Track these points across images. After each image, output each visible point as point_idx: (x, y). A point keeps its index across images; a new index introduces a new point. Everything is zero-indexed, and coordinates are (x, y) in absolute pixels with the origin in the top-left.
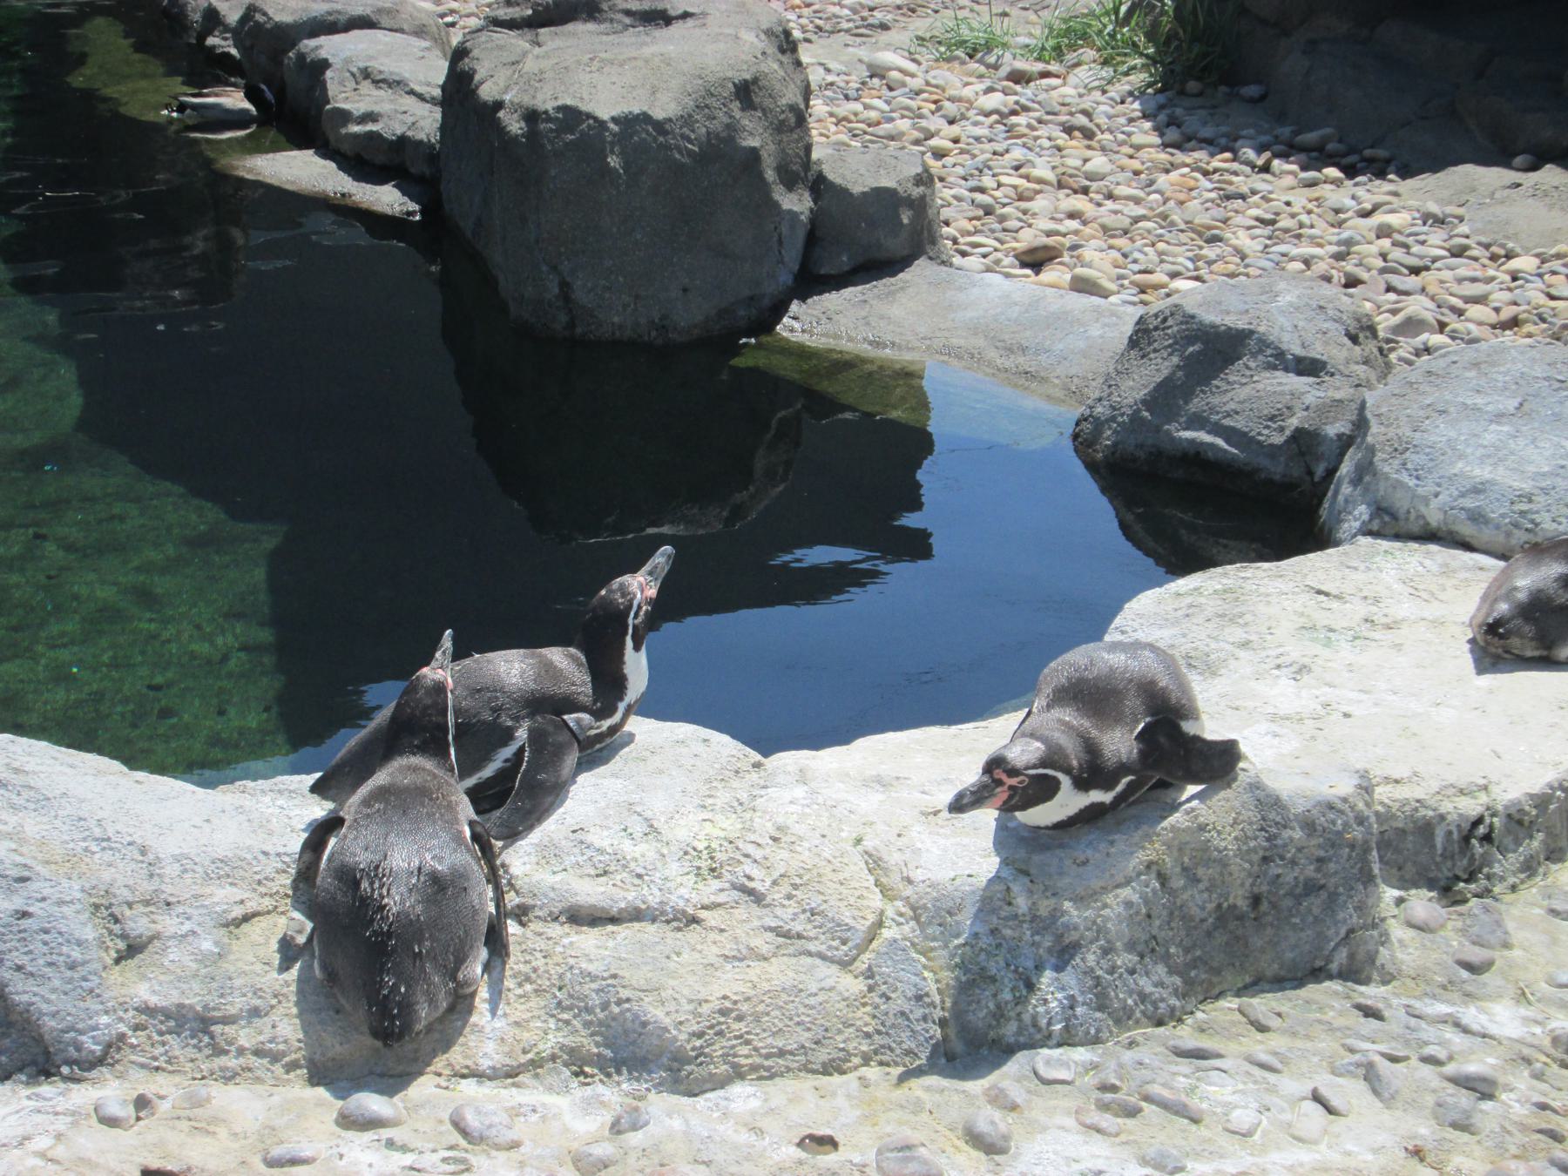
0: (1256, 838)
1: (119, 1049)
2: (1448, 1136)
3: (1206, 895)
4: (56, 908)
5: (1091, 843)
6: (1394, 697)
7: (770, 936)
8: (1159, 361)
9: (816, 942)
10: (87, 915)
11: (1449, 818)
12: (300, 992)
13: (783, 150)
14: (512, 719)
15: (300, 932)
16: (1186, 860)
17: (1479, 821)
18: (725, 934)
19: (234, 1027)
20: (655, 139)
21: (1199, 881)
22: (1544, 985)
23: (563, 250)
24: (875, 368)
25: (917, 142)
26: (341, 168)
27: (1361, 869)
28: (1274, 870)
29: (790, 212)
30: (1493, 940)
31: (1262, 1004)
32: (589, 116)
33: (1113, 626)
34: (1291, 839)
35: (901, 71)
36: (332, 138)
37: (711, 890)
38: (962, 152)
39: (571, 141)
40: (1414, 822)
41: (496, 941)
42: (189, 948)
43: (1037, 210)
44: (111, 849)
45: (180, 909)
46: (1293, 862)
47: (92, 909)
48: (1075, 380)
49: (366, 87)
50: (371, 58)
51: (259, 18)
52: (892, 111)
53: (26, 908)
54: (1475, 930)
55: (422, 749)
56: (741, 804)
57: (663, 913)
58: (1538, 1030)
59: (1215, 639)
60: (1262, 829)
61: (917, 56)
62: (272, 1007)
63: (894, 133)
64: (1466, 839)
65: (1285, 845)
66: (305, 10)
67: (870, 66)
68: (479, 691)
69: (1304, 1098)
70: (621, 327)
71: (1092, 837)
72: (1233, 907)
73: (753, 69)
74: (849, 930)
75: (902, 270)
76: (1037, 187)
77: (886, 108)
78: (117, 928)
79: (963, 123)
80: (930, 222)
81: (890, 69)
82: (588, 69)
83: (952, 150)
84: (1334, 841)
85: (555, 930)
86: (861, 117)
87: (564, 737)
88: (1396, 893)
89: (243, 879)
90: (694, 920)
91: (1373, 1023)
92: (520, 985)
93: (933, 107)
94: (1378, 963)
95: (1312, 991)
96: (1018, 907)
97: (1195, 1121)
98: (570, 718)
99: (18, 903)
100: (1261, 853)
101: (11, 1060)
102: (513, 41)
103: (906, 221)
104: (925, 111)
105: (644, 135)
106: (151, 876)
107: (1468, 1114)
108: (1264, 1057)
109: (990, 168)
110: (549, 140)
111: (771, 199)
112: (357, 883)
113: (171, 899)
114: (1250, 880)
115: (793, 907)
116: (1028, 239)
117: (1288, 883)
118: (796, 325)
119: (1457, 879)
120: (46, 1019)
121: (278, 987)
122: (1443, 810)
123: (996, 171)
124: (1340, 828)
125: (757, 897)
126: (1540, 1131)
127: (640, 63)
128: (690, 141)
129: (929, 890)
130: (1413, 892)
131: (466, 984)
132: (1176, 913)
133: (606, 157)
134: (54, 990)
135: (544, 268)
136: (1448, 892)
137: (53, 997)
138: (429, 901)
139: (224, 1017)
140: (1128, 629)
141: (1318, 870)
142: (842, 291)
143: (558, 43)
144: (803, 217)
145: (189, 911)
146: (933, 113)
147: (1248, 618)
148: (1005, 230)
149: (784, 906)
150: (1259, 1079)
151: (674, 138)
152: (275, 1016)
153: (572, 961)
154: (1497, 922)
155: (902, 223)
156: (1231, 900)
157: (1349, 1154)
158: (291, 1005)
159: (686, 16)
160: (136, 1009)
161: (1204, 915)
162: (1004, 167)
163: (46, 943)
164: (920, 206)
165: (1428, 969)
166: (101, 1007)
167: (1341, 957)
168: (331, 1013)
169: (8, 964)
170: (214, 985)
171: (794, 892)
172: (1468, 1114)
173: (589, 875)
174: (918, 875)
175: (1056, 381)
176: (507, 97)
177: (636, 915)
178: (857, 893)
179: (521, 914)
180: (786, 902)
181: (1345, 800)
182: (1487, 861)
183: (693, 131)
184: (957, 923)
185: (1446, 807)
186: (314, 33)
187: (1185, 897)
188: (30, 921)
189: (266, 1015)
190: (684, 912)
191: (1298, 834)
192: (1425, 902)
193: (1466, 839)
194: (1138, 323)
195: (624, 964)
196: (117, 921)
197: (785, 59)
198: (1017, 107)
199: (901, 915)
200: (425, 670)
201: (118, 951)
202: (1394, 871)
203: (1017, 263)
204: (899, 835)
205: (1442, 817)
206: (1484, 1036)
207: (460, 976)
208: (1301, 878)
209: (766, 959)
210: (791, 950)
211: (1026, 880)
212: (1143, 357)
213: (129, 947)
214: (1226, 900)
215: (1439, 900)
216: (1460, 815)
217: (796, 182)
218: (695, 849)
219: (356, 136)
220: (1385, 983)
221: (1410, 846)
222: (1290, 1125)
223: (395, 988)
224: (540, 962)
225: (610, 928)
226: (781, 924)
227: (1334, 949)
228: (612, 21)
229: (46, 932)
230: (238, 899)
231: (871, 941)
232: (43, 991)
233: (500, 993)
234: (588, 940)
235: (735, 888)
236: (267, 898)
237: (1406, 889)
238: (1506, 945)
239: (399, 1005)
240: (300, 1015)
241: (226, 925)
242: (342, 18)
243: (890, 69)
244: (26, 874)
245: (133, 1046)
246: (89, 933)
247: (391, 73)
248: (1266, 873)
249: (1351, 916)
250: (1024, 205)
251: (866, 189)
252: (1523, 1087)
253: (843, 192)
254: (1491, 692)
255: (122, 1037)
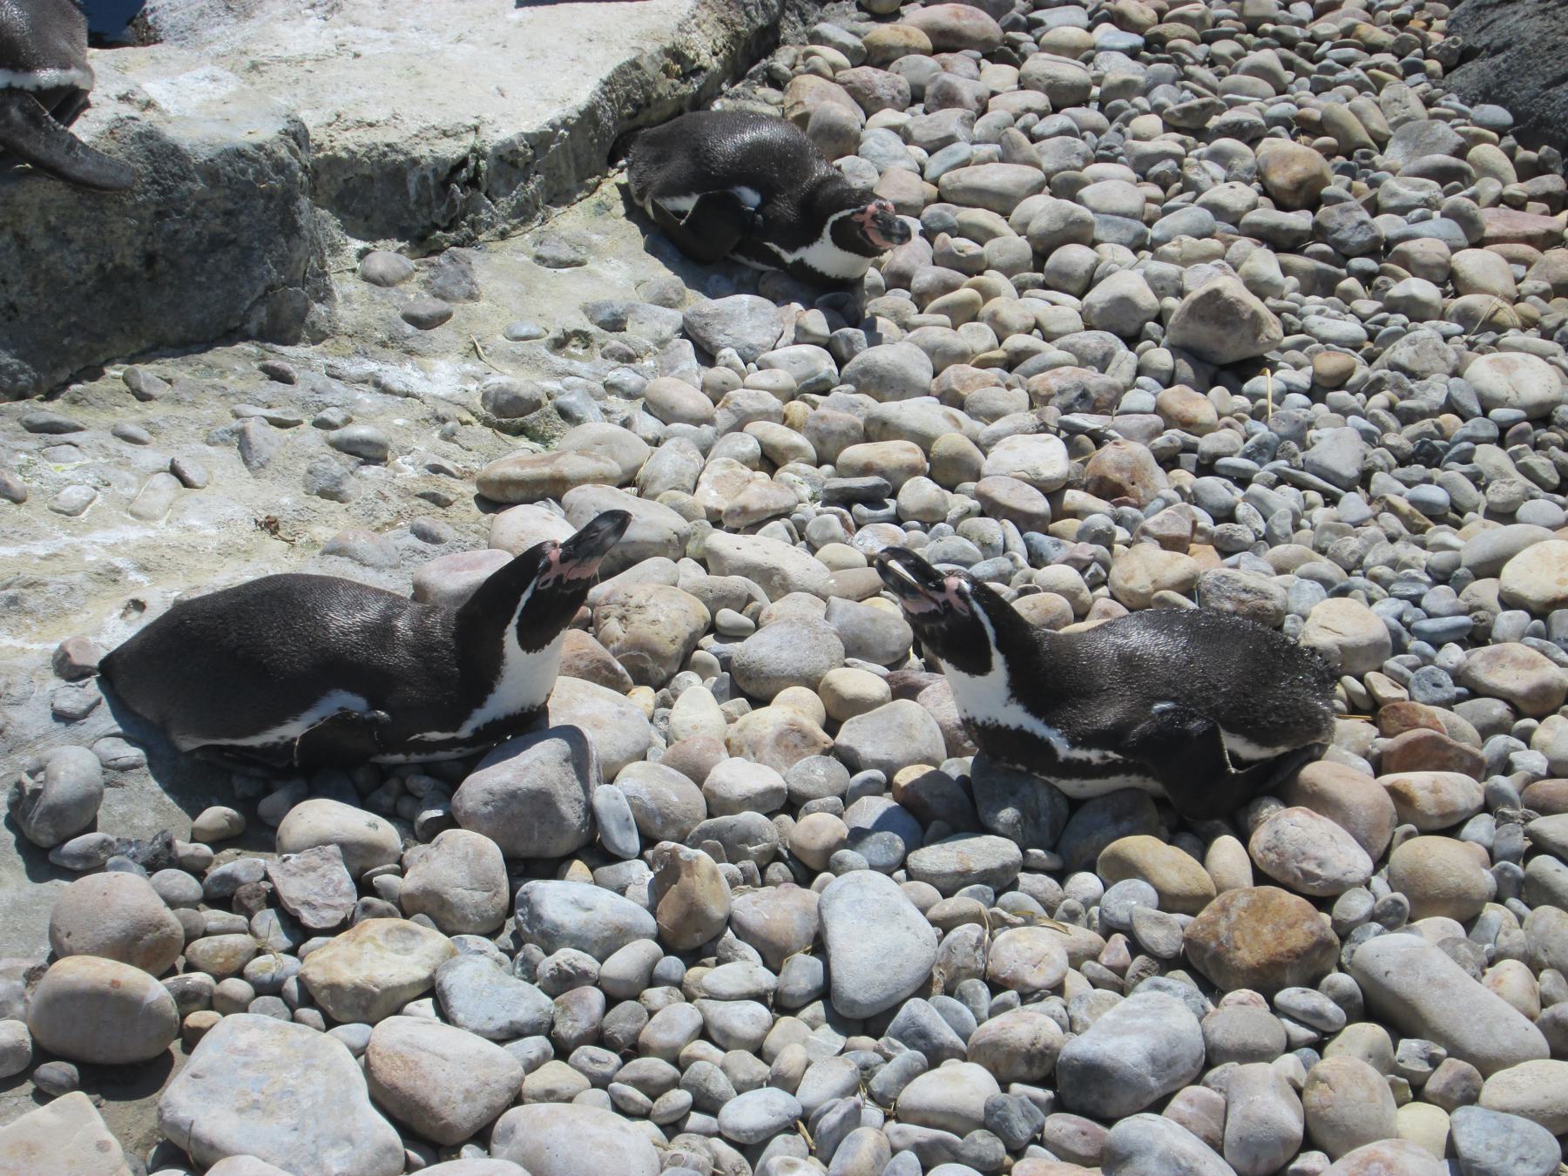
0: (145, 193)
2: (313, 505)
3: (82, 256)
6: (416, 35)
11: (423, 161)
16: (52, 219)
17: (463, 162)
22: (500, 338)
27: (282, 223)
28: (170, 225)
30: (456, 291)
31: (147, 373)
34: (191, 192)
40: (382, 168)
46: (194, 217)
54: (439, 281)
58: (472, 387)
60: (154, 182)
64: (444, 185)
65: (183, 199)
69: (160, 471)
72: (120, 268)
84: (243, 192)
88: (360, 245)
91: (278, 387)
94: (308, 321)
95: (219, 355)
97: (18, 501)
100: (153, 208)
107: (338, 481)
108: (131, 429)
114: (141, 238)
119: (437, 227)
122: (416, 154)
126: (423, 496)
130: (381, 242)
132: (41, 276)
136: (423, 243)
141: (226, 224)
150: (113, 452)
154: (463, 272)
156: (118, 261)
157: (189, 529)
161: (80, 277)
165: (369, 326)
167: (261, 315)
172: (338, 481)
181: (260, 147)
182: (472, 206)
185: (422, 151)
191: (199, 186)
192: (392, 254)
193: (444, 185)
202: (361, 221)
205: (415, 162)
206: (407, 395)
214: (110, 260)
215: (411, 250)
216: (436, 159)
220: (315, 342)
221: (378, 194)
222: (131, 501)
227: (251, 308)
237: (373, 240)
238: (472, 297)
249: (269, 272)
252: (422, 449)
254: (520, 24)
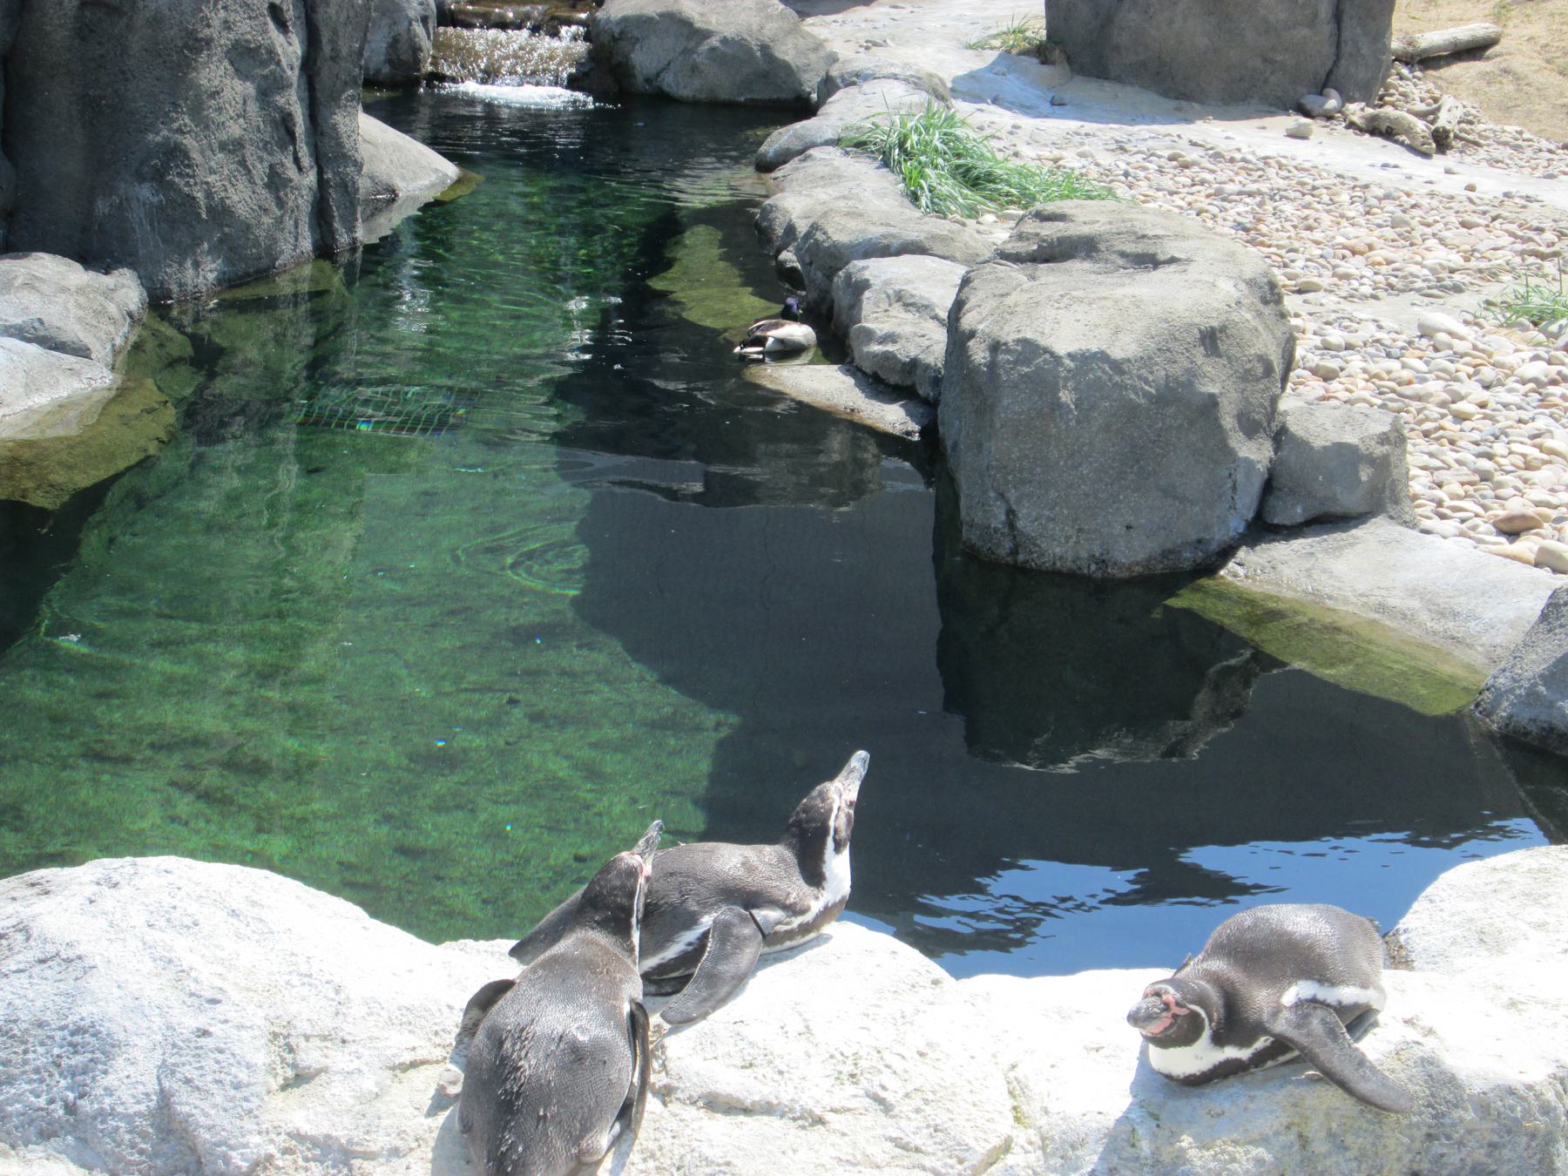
0: (1421, 1114)
1: (266, 1168)
4: (235, 1032)
5: (1231, 1096)
7: (889, 1145)
8: (1563, 636)
9: (933, 1158)
10: (264, 1041)
12: (440, 1139)
13: (1246, 399)
14: (698, 903)
15: (454, 1083)
16: (1334, 1125)
18: (846, 1138)
19: (373, 1163)
20: (1110, 379)
21: (1346, 1149)
23: (1010, 478)
24: (1305, 620)
25: (1443, 405)
26: (858, 385)
27: (1540, 1161)
29: (1246, 460)
32: (1046, 351)
33: (1424, 894)
34: (1461, 1120)
35: (1451, 334)
36: (856, 355)
37: (845, 1095)
38: (1485, 417)
39: (1026, 374)
41: (627, 1113)
42: (352, 1085)
43: (1536, 480)
44: (310, 985)
45: (353, 1048)
46: (1461, 1143)
47: (271, 1037)
48: (1499, 649)
49: (897, 310)
50: (909, 282)
51: (819, 236)
52: (1430, 372)
53: (207, 1027)
55: (602, 925)
56: (903, 1017)
57: (791, 1110)
59: (1514, 917)
60: (1429, 1105)
61: (1481, 320)
62: (411, 1150)
63: (1422, 393)
65: (1453, 1125)
66: (862, 231)
67: (1421, 326)
68: (672, 874)
70: (1061, 558)
71: (1233, 1090)
73: (1223, 317)
74: (968, 1150)
75: (1356, 527)
76: (1546, 457)
77: (1424, 368)
78: (289, 1058)
79: (1498, 389)
80: (1393, 481)
81: (1440, 330)
82: (1056, 305)
83: (1473, 415)
84: (1510, 1128)
85: (691, 1113)
86: (1393, 375)
87: (748, 930)
89: (422, 1028)
90: (820, 1121)
92: (645, 1160)
93: (1471, 370)
96: (1141, 1149)
98: (760, 914)
99: (202, 1021)
100: (1425, 1130)
101: (166, 1164)
102: (1013, 274)
103: (1364, 478)
104: (1462, 375)
105: (1099, 373)
106: (337, 1014)
109: (1507, 435)
110: (1006, 371)
111: (1226, 446)
112: (501, 1043)
113: (347, 1038)
114: (1410, 1156)
115: (918, 1120)
116: (1515, 506)
117: (1452, 1164)
118: (1241, 571)
120: (202, 1131)
121: (421, 1132)
123: (1511, 438)
124: (1519, 1115)
125: (885, 1106)
127: (1109, 303)
128: (1147, 382)
129: (1060, 1122)
131: (588, 1152)
133: (1059, 390)
134: (215, 1106)
135: (992, 494)
137: (213, 1112)
138: (564, 1068)
139: (365, 1153)
140: (1437, 899)
141: (1489, 1155)
142: (1292, 542)
143: (1051, 279)
144: (1259, 466)
145: (360, 1050)
146: (1470, 377)
147: (1553, 899)
148: (1497, 497)
149: (909, 1119)
151: (1131, 378)
152: (410, 1159)
153: (695, 1144)
155: (1360, 481)
158: (429, 1149)
159: (1173, 260)
160: (288, 1134)
162: (1522, 436)
163: (218, 1062)
164: (1382, 465)
166: (256, 1127)
168: (463, 1163)
169: (178, 1076)
170: (364, 1122)
171: (923, 1107)
173: (735, 1066)
174: (1053, 1108)
175: (1480, 649)
176: (981, 327)
177: (767, 1109)
178: (988, 1116)
179: (665, 1094)
180: (913, 1116)
181: (1530, 1088)
183: (1152, 373)
184: (1077, 1157)
186: (867, 255)
187: (1328, 1163)
188: (209, 1039)
189: (404, 1156)
190: (811, 1113)
191: (1470, 1115)
194: (1551, 597)
195: (741, 1153)
196: (291, 1050)
197: (1267, 311)
198: (1558, 378)
199: (1031, 1143)
200: (624, 854)
201: (285, 1079)
203: (1494, 530)
204: (1053, 1066)
207: (584, 1144)
208: (1469, 1161)
209: (878, 1167)
210: (906, 1162)
211: (1153, 1124)
212: (1550, 631)
213: (297, 1075)
217: (1257, 431)
218: (842, 1054)
219: (875, 355)
223: (513, 1147)
224: (666, 1142)
225: (742, 1118)
226: (901, 1135)
228: (1107, 261)
229: (221, 1051)
230: (410, 1045)
231: (991, 1165)
232: (205, 1105)
233: (624, 1165)
234: (719, 1126)
235: (868, 1096)
236: (439, 1049)
239: (515, 1164)
240: (433, 1161)
241: (393, 1068)
242: (896, 243)
243: (1440, 330)
244: (219, 997)
245: (278, 1168)
246: (261, 1058)
247: (922, 298)
248: (1427, 1150)
250: (1527, 474)
251: (1328, 444)
253: (1302, 445)
255: (270, 1157)
